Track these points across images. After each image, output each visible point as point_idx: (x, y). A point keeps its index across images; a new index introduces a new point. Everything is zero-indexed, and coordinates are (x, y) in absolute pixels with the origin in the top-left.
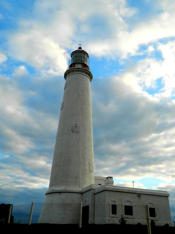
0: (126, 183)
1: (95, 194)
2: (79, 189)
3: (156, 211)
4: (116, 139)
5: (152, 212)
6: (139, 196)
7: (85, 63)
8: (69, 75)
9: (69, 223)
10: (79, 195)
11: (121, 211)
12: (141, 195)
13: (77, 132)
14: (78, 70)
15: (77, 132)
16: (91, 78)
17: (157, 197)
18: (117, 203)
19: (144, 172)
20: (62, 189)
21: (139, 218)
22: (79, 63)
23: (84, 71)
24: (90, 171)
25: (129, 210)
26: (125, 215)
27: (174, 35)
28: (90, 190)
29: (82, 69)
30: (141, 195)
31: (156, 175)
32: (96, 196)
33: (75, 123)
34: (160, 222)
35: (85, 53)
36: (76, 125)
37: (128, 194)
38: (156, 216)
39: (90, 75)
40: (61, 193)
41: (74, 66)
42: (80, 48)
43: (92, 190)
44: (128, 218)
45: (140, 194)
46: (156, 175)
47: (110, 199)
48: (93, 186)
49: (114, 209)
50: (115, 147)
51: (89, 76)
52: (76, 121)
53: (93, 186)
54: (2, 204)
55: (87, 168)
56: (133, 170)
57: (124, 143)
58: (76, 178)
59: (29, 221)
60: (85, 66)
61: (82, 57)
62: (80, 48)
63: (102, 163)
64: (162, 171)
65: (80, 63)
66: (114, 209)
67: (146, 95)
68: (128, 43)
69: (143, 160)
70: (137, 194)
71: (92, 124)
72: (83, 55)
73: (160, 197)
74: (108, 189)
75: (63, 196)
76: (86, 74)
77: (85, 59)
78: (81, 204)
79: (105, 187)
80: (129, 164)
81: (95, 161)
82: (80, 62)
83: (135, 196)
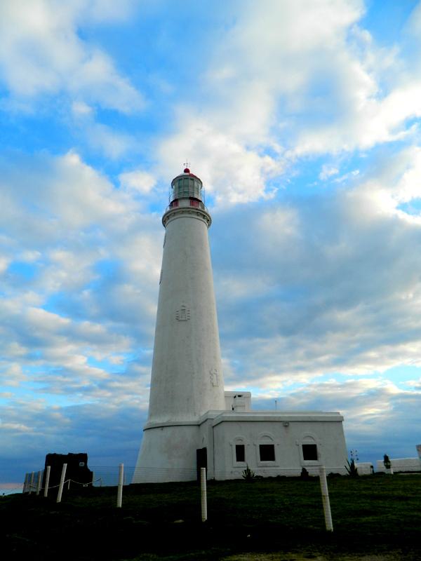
0: (359, 380)
1: (213, 427)
2: (194, 419)
3: (319, 450)
4: (346, 301)
5: (310, 452)
6: (286, 426)
7: (196, 197)
8: (173, 218)
9: (178, 480)
10: (195, 428)
11: (252, 455)
12: (290, 423)
13: (185, 320)
14: (184, 211)
15: (185, 320)
16: (209, 221)
17: (321, 424)
18: (246, 442)
19: (394, 356)
20: (165, 421)
21: (288, 463)
22: (183, 198)
23: (193, 212)
24: (213, 386)
25: (267, 453)
26: (261, 460)
27: (418, 115)
28: (206, 420)
29: (189, 208)
30: (290, 423)
31: (415, 361)
32: (215, 428)
33: (182, 304)
34: (326, 465)
35: (193, 178)
36: (183, 308)
37: (264, 423)
38: (319, 459)
39: (206, 217)
40: (165, 429)
41: (177, 204)
42: (187, 171)
43: (208, 421)
44: (267, 467)
45: (288, 422)
46: (415, 361)
47: (231, 437)
48: (210, 413)
49: (240, 452)
50: (342, 316)
51: (204, 218)
52: (183, 302)
53: (210, 413)
54: (69, 454)
55: (207, 380)
56: (373, 354)
57: (361, 307)
58: (188, 399)
59: (119, 479)
60: (194, 200)
61: (188, 186)
62: (187, 171)
63: (316, 347)
64: (271, 391)
65: (186, 198)
66: (240, 452)
67: (402, 215)
68: (375, 124)
69: (391, 333)
70: (281, 423)
71: (215, 302)
72: (190, 182)
73: (326, 424)
74: (242, 417)
75: (168, 431)
76: (198, 215)
77: (195, 190)
78: (120, 467)
79: (223, 417)
80: (367, 345)
81: (224, 364)
82: (186, 196)
83: (279, 426)
